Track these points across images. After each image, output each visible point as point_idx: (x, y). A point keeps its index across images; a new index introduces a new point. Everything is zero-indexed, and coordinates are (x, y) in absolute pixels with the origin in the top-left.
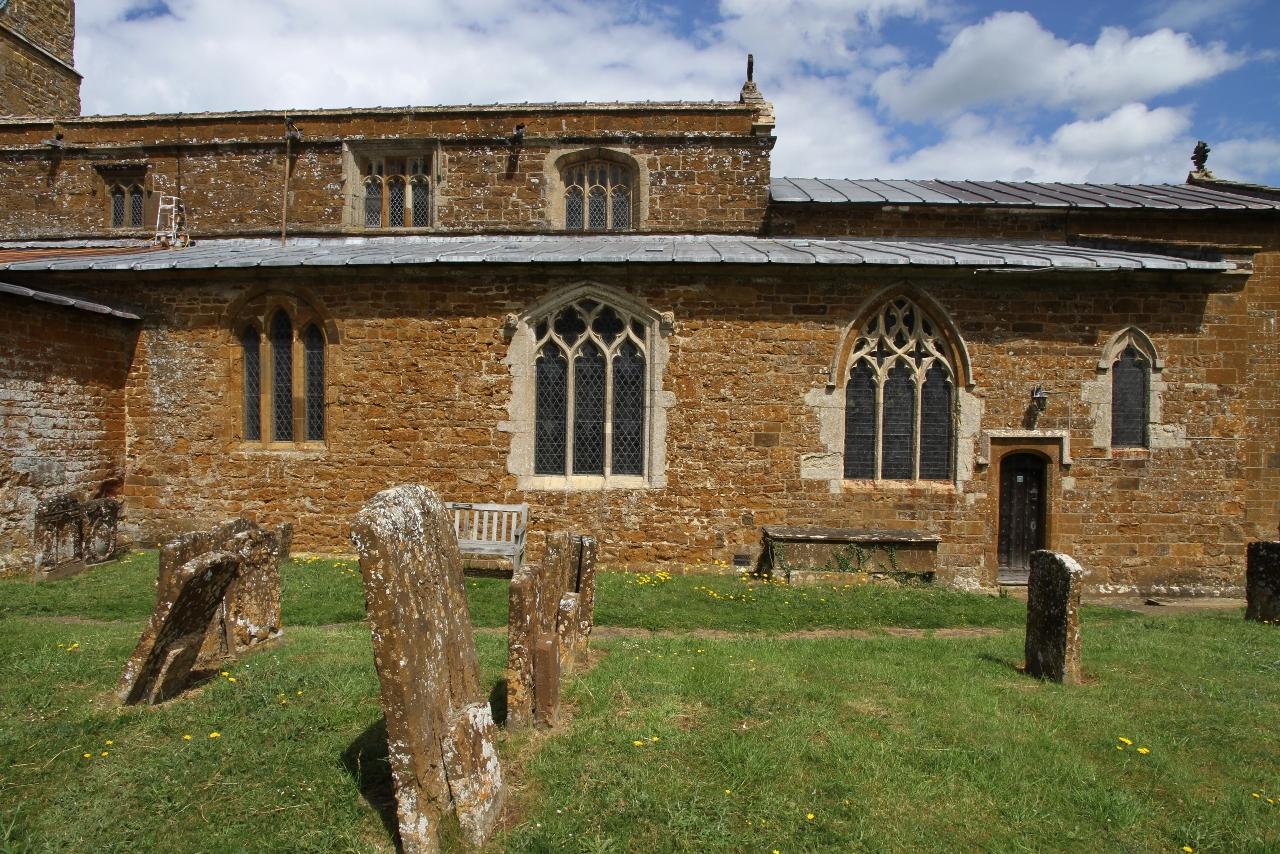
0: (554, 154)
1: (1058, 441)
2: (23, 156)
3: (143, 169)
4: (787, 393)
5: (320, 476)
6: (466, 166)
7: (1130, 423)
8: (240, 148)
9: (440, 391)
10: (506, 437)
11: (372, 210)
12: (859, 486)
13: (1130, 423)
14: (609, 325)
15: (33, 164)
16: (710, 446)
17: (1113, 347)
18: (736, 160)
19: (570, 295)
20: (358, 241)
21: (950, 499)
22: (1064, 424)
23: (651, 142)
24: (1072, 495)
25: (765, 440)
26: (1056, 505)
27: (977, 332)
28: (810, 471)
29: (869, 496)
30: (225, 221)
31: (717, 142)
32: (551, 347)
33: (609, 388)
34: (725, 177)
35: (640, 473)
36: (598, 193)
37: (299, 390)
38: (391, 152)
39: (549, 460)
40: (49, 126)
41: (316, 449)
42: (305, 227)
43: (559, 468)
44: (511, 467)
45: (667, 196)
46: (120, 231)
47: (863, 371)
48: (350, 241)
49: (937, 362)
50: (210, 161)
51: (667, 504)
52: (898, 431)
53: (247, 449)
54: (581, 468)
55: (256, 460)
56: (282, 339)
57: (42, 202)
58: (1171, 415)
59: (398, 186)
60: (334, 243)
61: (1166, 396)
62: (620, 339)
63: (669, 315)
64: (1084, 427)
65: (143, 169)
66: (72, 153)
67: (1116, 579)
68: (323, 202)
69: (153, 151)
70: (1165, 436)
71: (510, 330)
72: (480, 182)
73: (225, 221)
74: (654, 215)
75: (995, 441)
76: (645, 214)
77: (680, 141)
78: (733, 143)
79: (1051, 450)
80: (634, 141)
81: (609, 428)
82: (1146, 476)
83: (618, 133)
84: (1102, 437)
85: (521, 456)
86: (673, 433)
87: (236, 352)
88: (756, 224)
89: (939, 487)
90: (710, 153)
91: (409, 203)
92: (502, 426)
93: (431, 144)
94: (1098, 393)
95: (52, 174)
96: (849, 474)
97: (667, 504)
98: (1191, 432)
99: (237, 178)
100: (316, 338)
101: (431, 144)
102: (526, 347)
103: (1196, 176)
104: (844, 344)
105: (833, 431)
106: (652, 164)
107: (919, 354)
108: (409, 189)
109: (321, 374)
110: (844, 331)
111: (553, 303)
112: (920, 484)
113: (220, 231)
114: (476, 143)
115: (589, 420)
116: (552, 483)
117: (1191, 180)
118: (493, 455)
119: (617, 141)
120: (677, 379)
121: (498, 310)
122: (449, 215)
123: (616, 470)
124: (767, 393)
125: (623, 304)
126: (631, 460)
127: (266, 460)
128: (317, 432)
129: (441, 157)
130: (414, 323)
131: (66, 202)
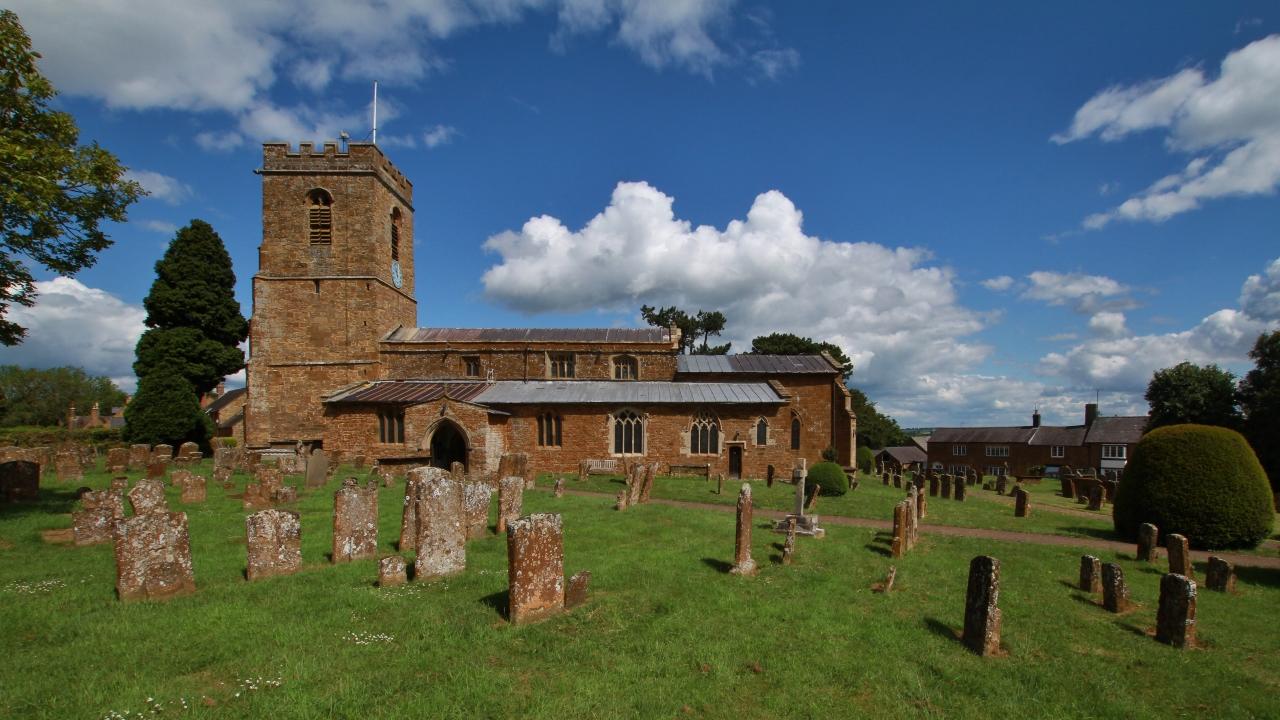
0: (611, 357)
2: (420, 353)
3: (479, 358)
4: (676, 433)
7: (762, 439)
8: (511, 352)
10: (608, 444)
11: (554, 372)
13: (762, 439)
14: (633, 417)
15: (439, 355)
17: (757, 420)
18: (667, 359)
19: (623, 410)
20: (550, 382)
21: (717, 458)
25: (671, 444)
26: (743, 459)
27: (723, 418)
28: (682, 451)
29: (696, 458)
31: (661, 353)
32: (619, 422)
35: (640, 452)
36: (625, 368)
37: (554, 433)
39: (618, 450)
46: (470, 377)
47: (695, 427)
50: (501, 356)
52: (704, 441)
54: (626, 451)
57: (442, 368)
59: (562, 365)
64: (750, 440)
65: (479, 358)
66: (453, 352)
67: (759, 477)
69: (480, 352)
70: (770, 442)
71: (608, 418)
72: (589, 364)
74: (642, 375)
76: (640, 375)
77: (650, 353)
80: (636, 353)
82: (765, 452)
84: (755, 442)
85: (612, 449)
86: (649, 443)
87: (536, 423)
89: (714, 455)
90: (659, 356)
94: (754, 432)
95: (444, 358)
96: (692, 452)
102: (612, 422)
106: (641, 360)
110: (690, 418)
111: (619, 412)
112: (709, 454)
114: (587, 353)
120: (651, 429)
122: (580, 375)
126: (639, 449)
128: (559, 443)
130: (584, 417)
131: (452, 368)
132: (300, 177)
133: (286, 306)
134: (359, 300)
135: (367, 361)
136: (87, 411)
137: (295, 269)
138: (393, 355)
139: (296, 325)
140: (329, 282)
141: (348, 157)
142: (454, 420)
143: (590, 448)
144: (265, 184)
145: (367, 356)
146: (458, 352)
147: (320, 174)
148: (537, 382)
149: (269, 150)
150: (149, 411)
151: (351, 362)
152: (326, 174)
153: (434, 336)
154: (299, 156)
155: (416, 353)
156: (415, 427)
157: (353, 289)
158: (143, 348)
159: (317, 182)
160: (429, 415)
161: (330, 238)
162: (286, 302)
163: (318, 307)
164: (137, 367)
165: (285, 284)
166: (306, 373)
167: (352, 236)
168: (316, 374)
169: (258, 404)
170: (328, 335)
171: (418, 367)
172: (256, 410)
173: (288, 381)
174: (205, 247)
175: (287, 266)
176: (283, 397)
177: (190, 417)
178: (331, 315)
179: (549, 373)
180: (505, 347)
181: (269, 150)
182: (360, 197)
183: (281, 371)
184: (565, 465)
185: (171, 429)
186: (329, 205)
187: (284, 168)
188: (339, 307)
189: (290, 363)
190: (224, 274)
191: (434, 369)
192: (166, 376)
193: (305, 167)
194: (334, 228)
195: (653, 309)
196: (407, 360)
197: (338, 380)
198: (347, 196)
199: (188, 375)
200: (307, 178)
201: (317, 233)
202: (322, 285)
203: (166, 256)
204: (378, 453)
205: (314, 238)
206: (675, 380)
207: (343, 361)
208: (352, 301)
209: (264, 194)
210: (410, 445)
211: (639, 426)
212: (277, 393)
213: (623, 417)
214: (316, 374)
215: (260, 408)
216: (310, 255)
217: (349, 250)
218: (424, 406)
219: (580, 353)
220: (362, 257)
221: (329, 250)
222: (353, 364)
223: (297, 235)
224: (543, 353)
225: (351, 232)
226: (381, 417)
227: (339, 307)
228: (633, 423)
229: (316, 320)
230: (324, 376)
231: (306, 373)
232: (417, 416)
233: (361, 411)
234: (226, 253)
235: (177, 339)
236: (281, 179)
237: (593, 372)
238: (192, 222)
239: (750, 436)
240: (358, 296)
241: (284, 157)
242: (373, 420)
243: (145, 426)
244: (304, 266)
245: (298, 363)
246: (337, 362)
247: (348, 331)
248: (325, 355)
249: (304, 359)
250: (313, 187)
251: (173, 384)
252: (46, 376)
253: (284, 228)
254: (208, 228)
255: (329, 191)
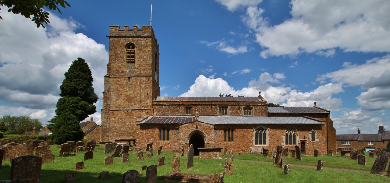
0: (243, 107)
1: (306, 141)
2: (175, 105)
5: (234, 145)
6: (232, 108)
7: (313, 139)
9: (246, 136)
11: (220, 113)
12: (287, 145)
13: (313, 139)
14: (263, 130)
16: (273, 141)
17: (311, 132)
18: (264, 108)
19: (259, 127)
20: (220, 117)
22: (307, 139)
23: (255, 106)
24: (308, 146)
25: (278, 141)
26: (306, 147)
28: (282, 144)
30: (202, 114)
31: (262, 106)
33: (292, 141)
34: (263, 109)
37: (231, 136)
38: (223, 106)
39: (257, 143)
40: (178, 101)
41: (233, 142)
42: (212, 115)
43: (258, 144)
44: (253, 144)
45: (256, 112)
46: (188, 115)
48: (219, 117)
49: (294, 133)
50: (200, 106)
51: (269, 147)
52: (290, 139)
53: (225, 142)
54: (260, 144)
55: (226, 144)
56: (229, 131)
57: (177, 111)
58: (317, 138)
59: (223, 110)
60: (217, 117)
61: (317, 136)
62: (264, 131)
63: (269, 129)
64: (309, 139)
66: (182, 105)
68: (215, 112)
69: (192, 105)
70: (317, 140)
71: (254, 130)
72: (234, 110)
73: (202, 114)
74: (255, 114)
75: (300, 141)
78: (264, 106)
79: (306, 141)
80: (252, 105)
81: (263, 140)
83: (251, 104)
84: (311, 140)
88: (267, 115)
91: (225, 112)
92: (252, 140)
93: (228, 105)
94: (310, 136)
97: (269, 147)
98: (319, 139)
99: (204, 108)
100: (232, 131)
101: (228, 105)
102: (255, 132)
103: (315, 106)
104: (285, 132)
105: (285, 140)
106: (254, 108)
107: (292, 132)
108: (225, 110)
109: (233, 135)
111: (258, 128)
113: (202, 115)
114: (234, 105)
115: (261, 139)
116: (257, 145)
117: (314, 106)
118: (252, 143)
119: (250, 105)
120: (270, 135)
121: (252, 128)
123: (263, 144)
124: (278, 136)
125: (264, 128)
126: (265, 143)
127: (228, 144)
129: (229, 107)
130: (244, 130)
132: (124, 38)
133: (117, 87)
134: (145, 85)
135: (148, 108)
136: (31, 130)
137: (121, 73)
138: (158, 106)
139: (121, 94)
140: (134, 78)
141: (142, 31)
142: (200, 130)
143: (246, 143)
144: (110, 41)
145: (148, 107)
146: (183, 105)
147: (132, 37)
148: (214, 117)
149: (112, 28)
150: (61, 128)
151: (142, 109)
152: (134, 37)
153: (172, 99)
154: (123, 31)
155: (167, 105)
156: (184, 134)
157: (143, 81)
158: (60, 104)
159: (130, 40)
160: (190, 128)
161: (134, 61)
162: (117, 86)
163: (129, 87)
164: (58, 112)
165: (117, 79)
166: (125, 113)
167: (143, 61)
168: (129, 113)
169: (106, 125)
170: (133, 98)
171: (168, 111)
172: (105, 127)
173: (117, 116)
174: (83, 67)
175: (118, 72)
176: (115, 123)
177: (77, 130)
178: (134, 91)
179: (218, 113)
180: (202, 103)
181: (112, 28)
182: (147, 46)
183: (114, 112)
184: (236, 150)
185: (70, 135)
186: (134, 49)
187: (117, 35)
188: (137, 88)
189: (118, 109)
190: (89, 77)
191: (174, 111)
192: (68, 114)
193: (125, 35)
194: (136, 58)
195: (223, 95)
196: (164, 108)
197: (137, 116)
198: (141, 46)
199: (76, 115)
200: (126, 39)
201: (130, 59)
202: (131, 79)
203: (68, 71)
204: (159, 145)
205: (129, 62)
206: (268, 116)
207: (139, 108)
208: (143, 85)
209: (110, 45)
210: (182, 142)
211: (265, 133)
212: (113, 121)
213: (259, 130)
214: (129, 113)
215: (106, 127)
216: (127, 68)
217: (142, 66)
218: (188, 124)
219: (231, 105)
220: (147, 69)
221: (134, 66)
222: (143, 110)
223: (122, 60)
224: (216, 105)
225: (143, 59)
226: (160, 130)
227: (137, 88)
228: (263, 132)
229: (129, 92)
230: (132, 114)
231: (125, 113)
232: (184, 129)
233: (152, 128)
234: (90, 70)
235: (72, 100)
236: (116, 39)
237: (236, 112)
238: (78, 58)
239: (309, 137)
240: (145, 83)
241: (118, 31)
242: (157, 131)
243: (60, 134)
244: (124, 72)
245: (121, 109)
246: (136, 109)
247: (141, 97)
248: (132, 106)
249: (124, 108)
250: (128, 42)
251: (71, 117)
252: (18, 119)
253: (117, 57)
254: (83, 61)
255: (134, 43)
